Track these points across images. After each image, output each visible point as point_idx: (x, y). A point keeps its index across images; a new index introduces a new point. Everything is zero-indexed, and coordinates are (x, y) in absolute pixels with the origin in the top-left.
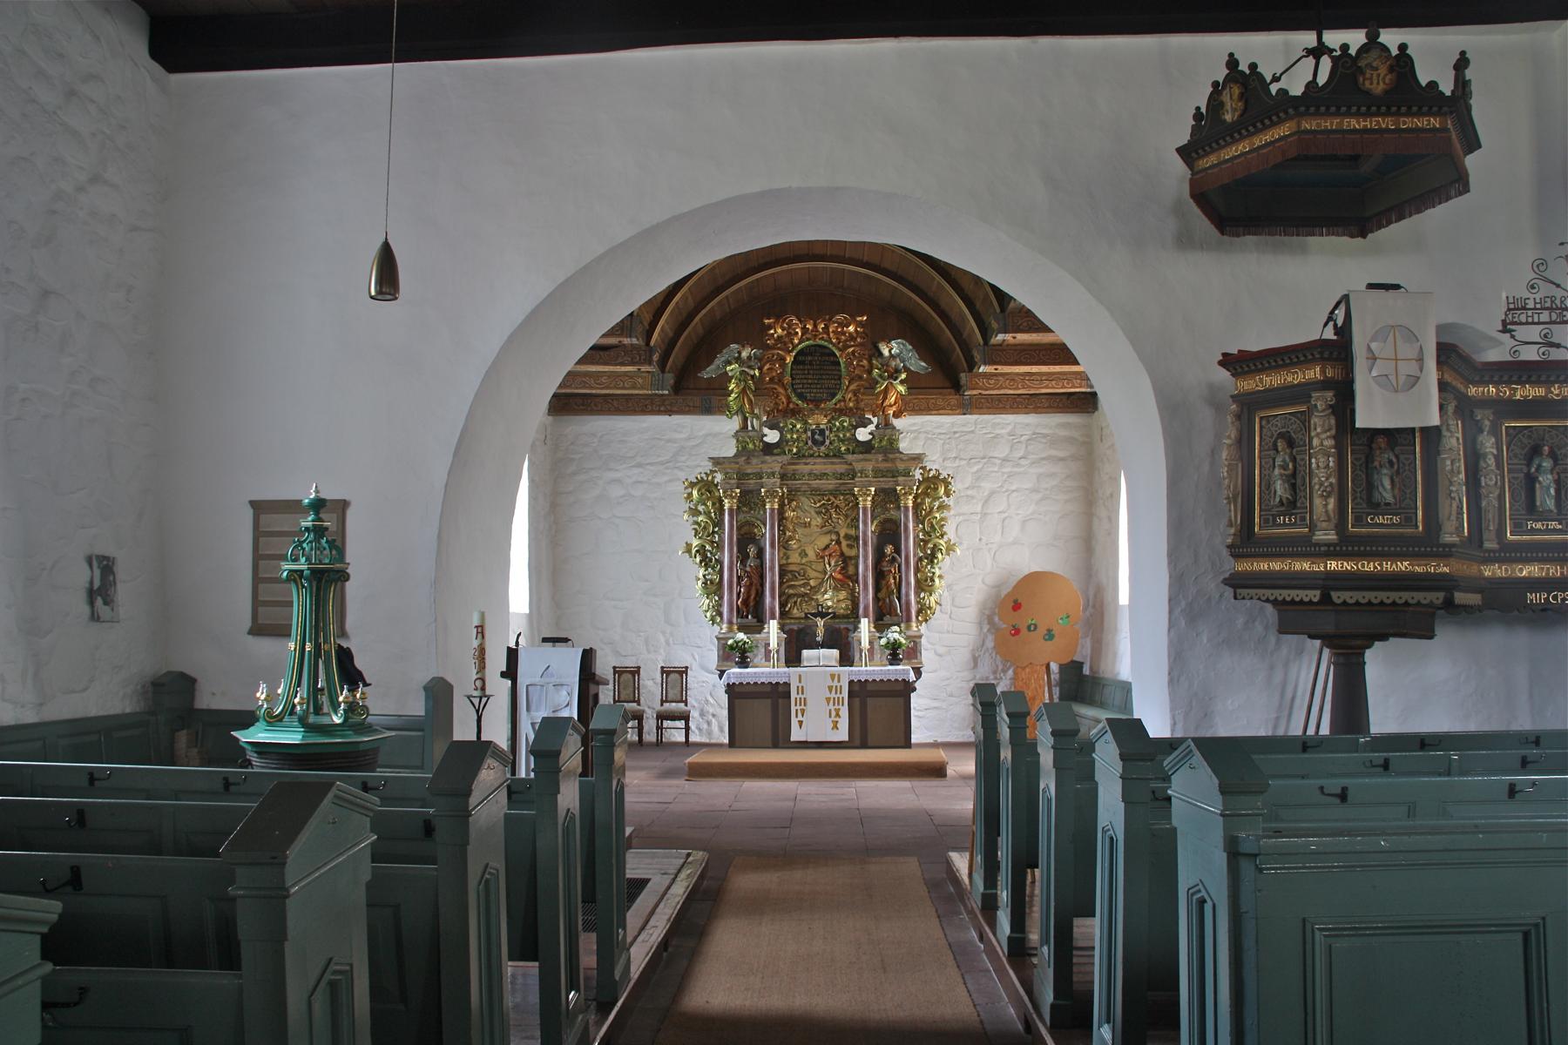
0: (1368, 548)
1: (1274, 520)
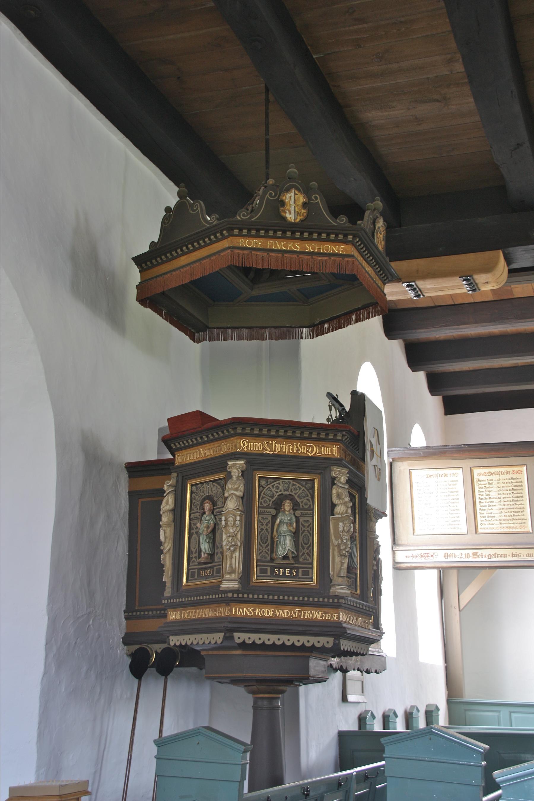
0: (316, 599)
1: (273, 572)
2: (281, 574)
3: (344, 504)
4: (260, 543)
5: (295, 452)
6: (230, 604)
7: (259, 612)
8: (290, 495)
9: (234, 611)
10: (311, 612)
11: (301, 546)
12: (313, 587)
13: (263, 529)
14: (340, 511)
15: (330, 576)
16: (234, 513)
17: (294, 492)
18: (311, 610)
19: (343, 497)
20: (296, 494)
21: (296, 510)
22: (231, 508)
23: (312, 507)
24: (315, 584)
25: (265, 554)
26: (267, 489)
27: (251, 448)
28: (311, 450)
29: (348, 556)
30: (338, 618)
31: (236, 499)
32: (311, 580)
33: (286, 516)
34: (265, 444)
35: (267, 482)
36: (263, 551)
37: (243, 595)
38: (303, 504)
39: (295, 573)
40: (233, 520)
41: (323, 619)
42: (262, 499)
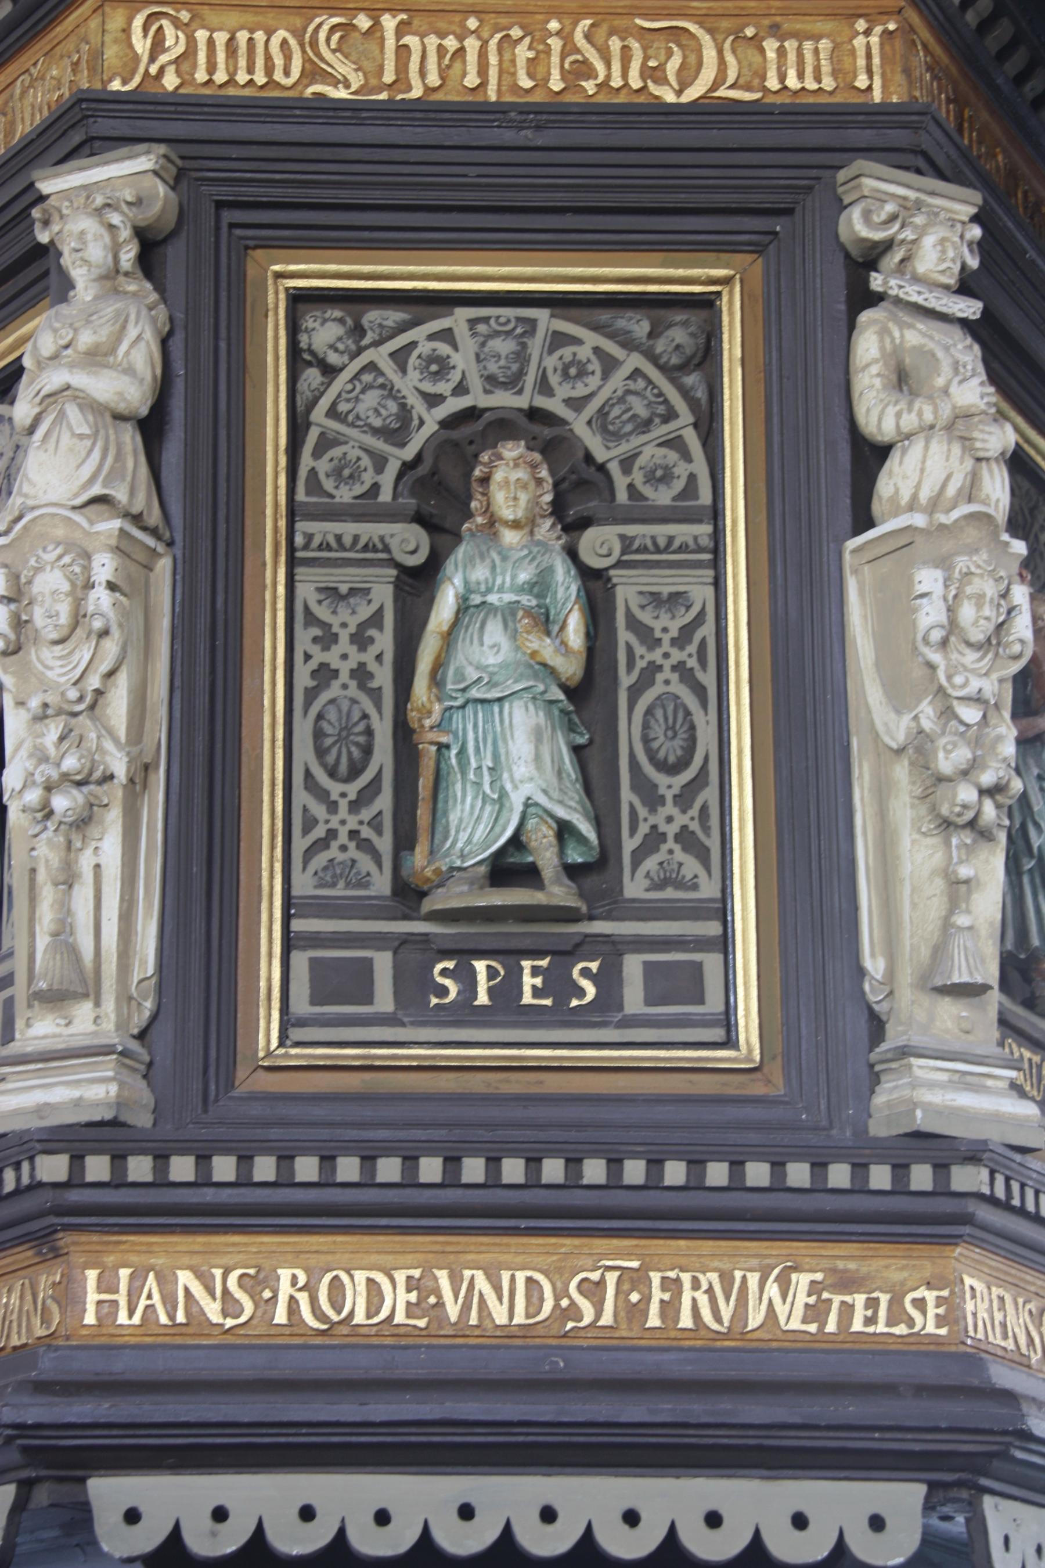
2: (482, 998)
3: (949, 427)
4: (308, 774)
5: (556, 84)
6: (65, 1239)
7: (303, 1298)
8: (534, 414)
9: (92, 1297)
10: (726, 1279)
11: (634, 787)
12: (732, 1086)
13: (336, 673)
14: (918, 486)
15: (863, 993)
16: (78, 535)
17: (563, 391)
18: (726, 1266)
19: (940, 382)
20: (576, 404)
21: (584, 523)
22: (52, 497)
23: (705, 497)
24: (749, 1059)
25: (353, 852)
26: (356, 377)
27: (211, 68)
28: (683, 67)
29: (1002, 837)
30: (951, 1316)
31: (86, 430)
32: (717, 1034)
33: (504, 559)
34: (322, 35)
35: (358, 331)
36: (332, 834)
37: (161, 1159)
38: (637, 477)
39: (591, 991)
40: (66, 587)
41: (831, 1327)
42: (317, 454)
